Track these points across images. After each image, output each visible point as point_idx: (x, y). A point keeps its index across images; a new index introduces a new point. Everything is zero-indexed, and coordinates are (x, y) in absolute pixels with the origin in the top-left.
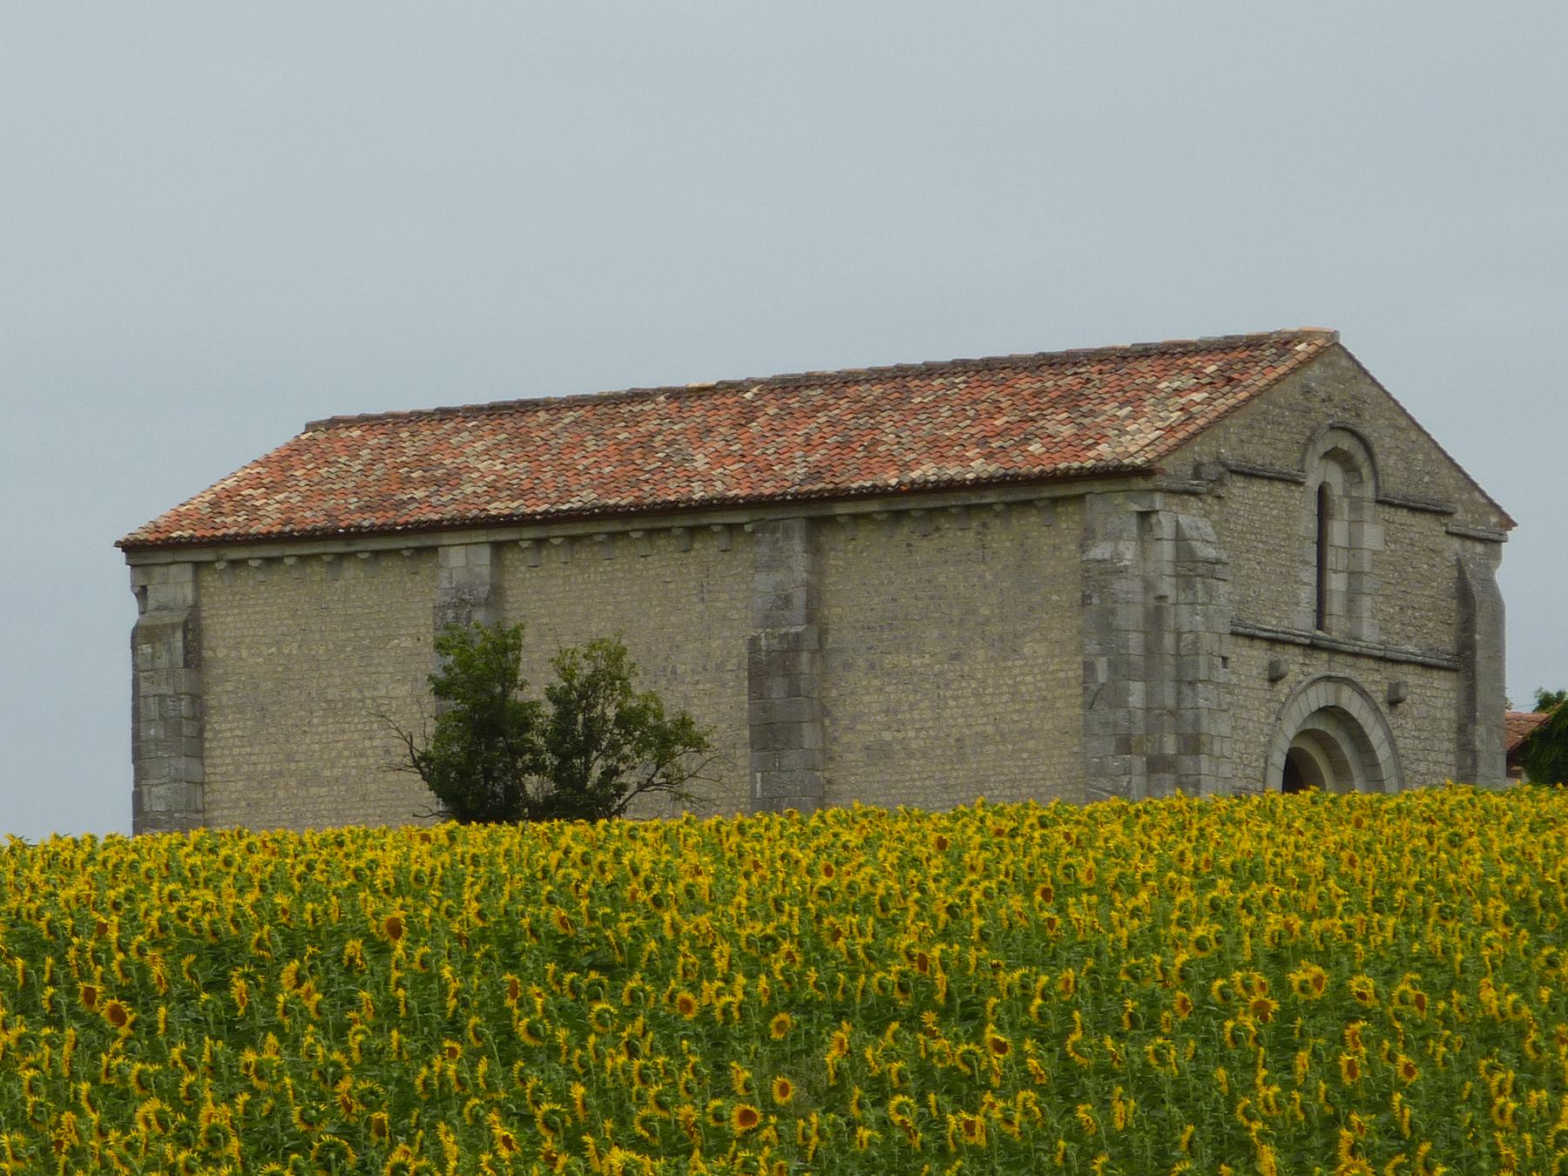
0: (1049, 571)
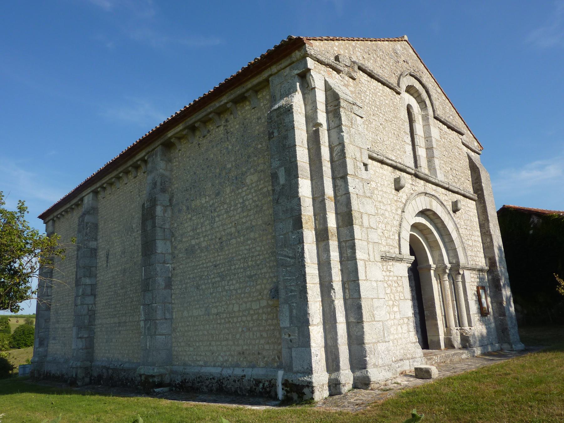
0: (257, 132)
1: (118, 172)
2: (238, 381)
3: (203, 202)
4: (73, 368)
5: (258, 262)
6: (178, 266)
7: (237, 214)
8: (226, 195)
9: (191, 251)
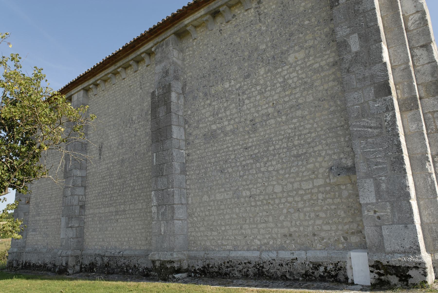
0: (302, 9)
1: (116, 67)
4: (63, 257)
5: (309, 140)
7: (276, 93)
8: (259, 76)
9: (211, 136)
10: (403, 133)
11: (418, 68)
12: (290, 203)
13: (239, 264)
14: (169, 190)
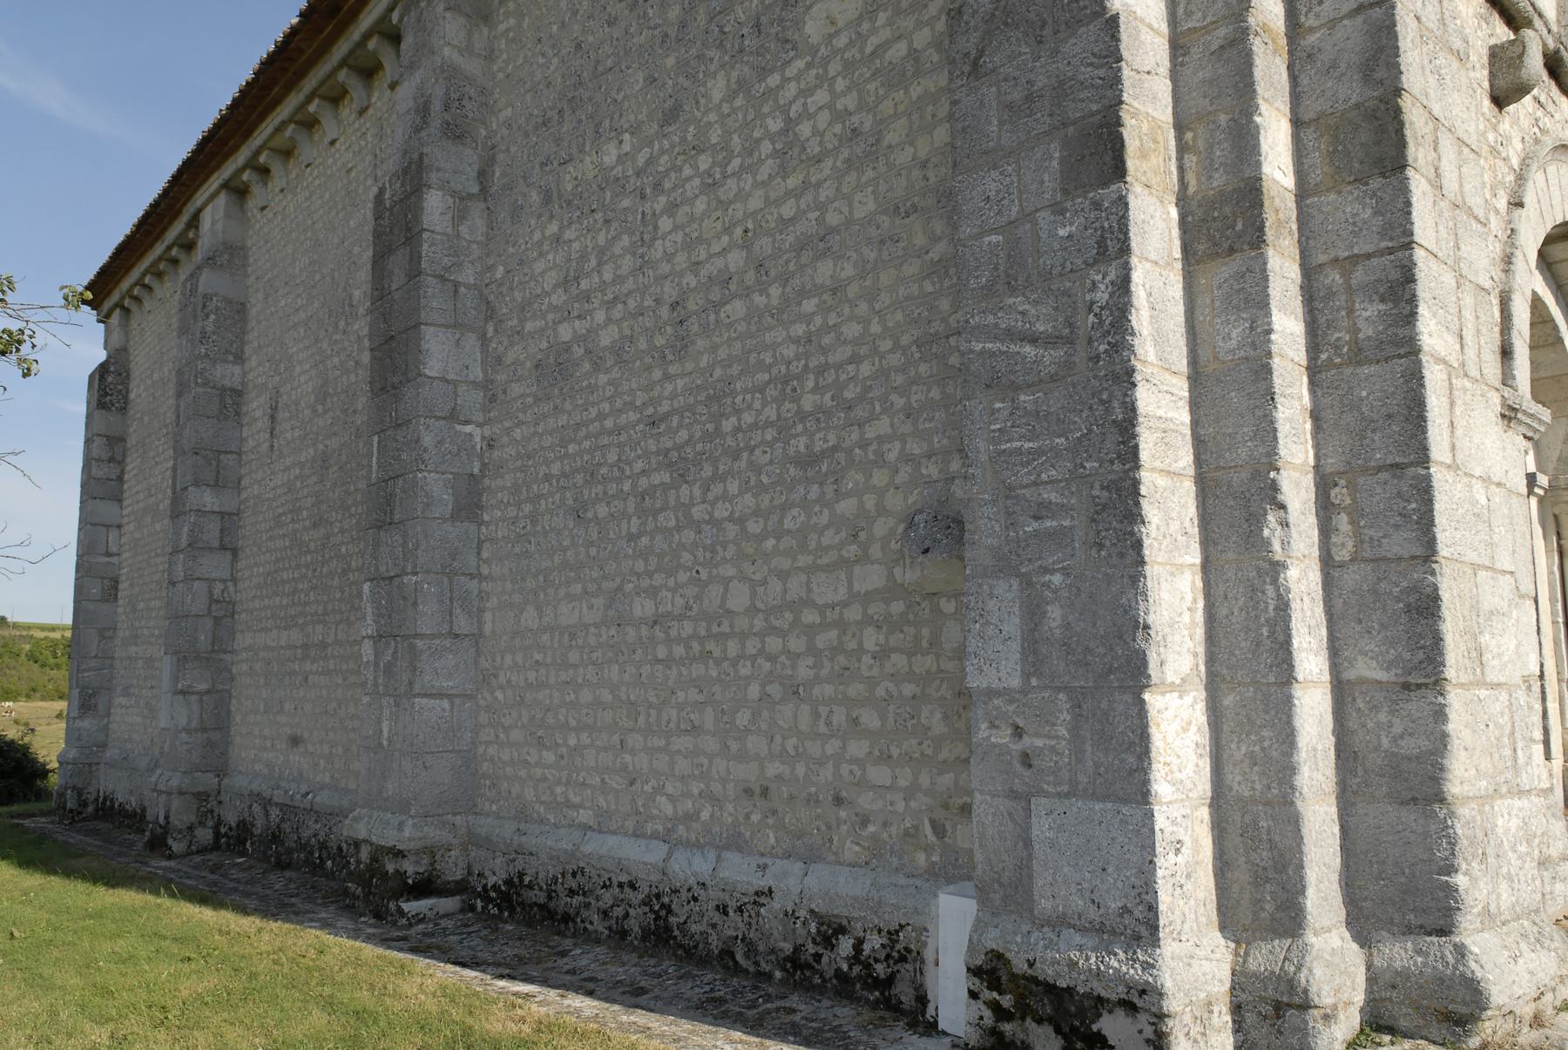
2: (740, 910)
3: (610, 158)
6: (508, 431)
7: (756, 185)
9: (555, 369)
10: (1182, 365)
11: (1312, 39)
12: (772, 658)
13: (605, 886)
14: (406, 580)
